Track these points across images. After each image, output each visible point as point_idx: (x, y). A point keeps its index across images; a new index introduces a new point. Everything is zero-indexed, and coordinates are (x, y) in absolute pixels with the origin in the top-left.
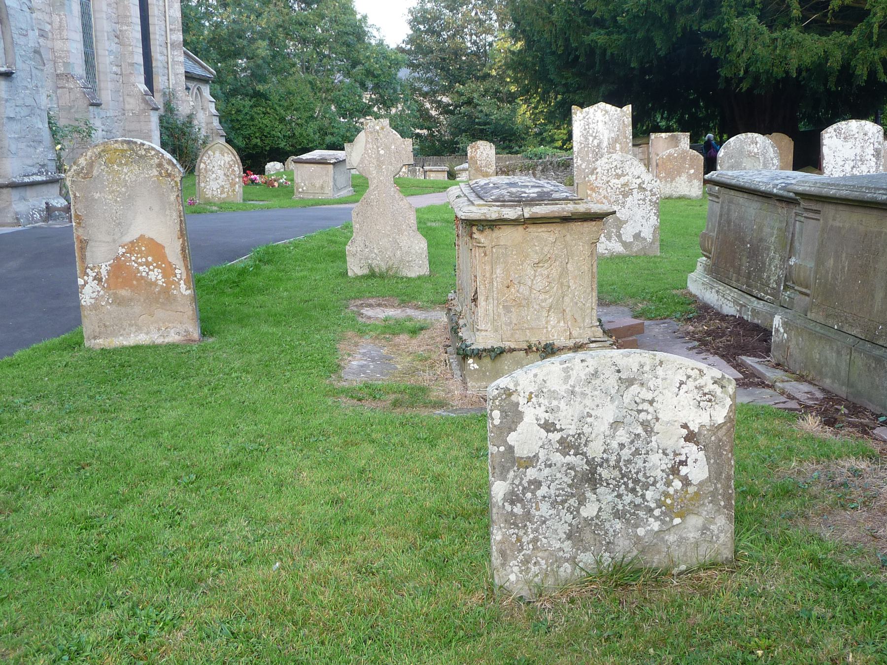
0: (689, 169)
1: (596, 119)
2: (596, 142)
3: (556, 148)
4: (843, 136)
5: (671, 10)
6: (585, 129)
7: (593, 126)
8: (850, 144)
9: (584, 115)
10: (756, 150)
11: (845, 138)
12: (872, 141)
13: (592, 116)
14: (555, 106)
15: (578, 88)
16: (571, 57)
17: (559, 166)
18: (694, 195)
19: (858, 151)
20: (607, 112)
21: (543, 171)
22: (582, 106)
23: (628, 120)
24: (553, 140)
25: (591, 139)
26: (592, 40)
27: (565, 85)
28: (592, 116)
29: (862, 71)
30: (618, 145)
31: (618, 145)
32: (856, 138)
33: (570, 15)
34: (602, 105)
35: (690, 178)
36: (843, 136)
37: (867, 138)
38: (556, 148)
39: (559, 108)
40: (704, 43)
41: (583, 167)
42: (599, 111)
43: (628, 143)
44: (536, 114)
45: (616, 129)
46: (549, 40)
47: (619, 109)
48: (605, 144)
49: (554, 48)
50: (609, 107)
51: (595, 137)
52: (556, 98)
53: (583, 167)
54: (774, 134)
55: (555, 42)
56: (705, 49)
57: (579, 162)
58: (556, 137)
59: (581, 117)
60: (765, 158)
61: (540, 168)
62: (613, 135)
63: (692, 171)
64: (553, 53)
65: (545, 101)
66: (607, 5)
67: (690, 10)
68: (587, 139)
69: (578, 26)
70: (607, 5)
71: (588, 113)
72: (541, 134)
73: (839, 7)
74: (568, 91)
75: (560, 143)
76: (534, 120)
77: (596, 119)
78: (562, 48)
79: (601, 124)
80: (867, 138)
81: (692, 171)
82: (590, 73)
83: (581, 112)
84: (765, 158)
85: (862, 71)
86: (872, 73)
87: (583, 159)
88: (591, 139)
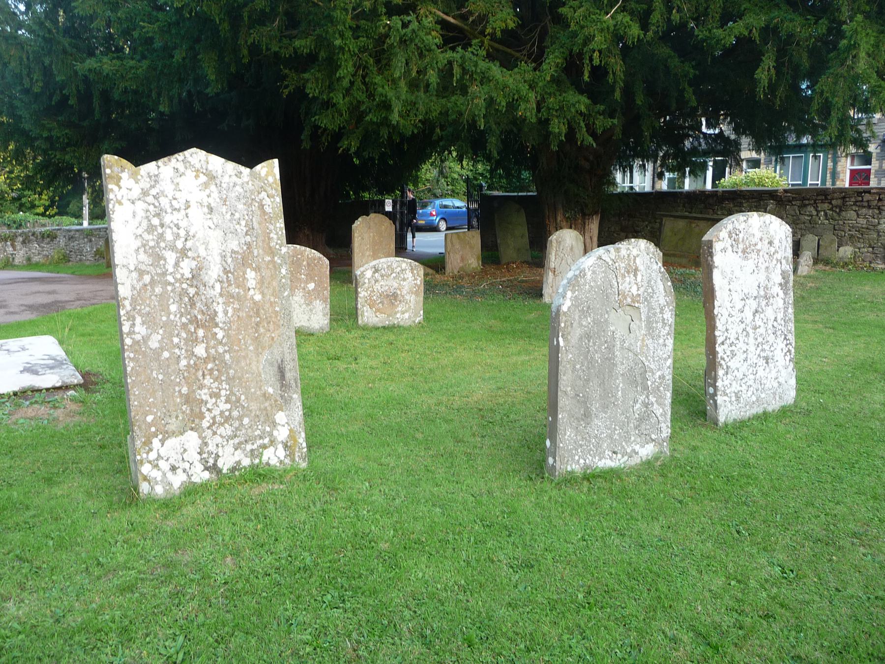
0: (307, 283)
1: (182, 197)
2: (186, 267)
3: (38, 214)
4: (741, 246)
5: (234, 15)
6: (151, 229)
7: (176, 217)
8: (750, 264)
9: (145, 184)
10: (634, 291)
11: (744, 252)
12: (778, 256)
13: (169, 189)
14: (35, 168)
15: (68, 145)
16: (56, 99)
17: (43, 237)
18: (317, 326)
19: (762, 277)
20: (211, 177)
21: (24, 242)
22: (139, 153)
23: (274, 202)
24: (33, 206)
25: (171, 257)
26: (90, 70)
27: (49, 139)
28: (169, 189)
29: (558, 127)
30: (251, 274)
31: (251, 274)
32: (759, 251)
33: (50, 31)
34: (196, 156)
35: (309, 297)
36: (741, 246)
37: (772, 250)
38: (38, 214)
39: (40, 171)
40: (285, 77)
41: (154, 343)
42: (190, 174)
43: (277, 268)
44: (12, 179)
45: (242, 228)
46: (17, 71)
47: (246, 171)
48: (214, 272)
49: (27, 83)
50: (216, 162)
51: (183, 253)
52: (34, 159)
53: (154, 343)
54: (372, 215)
55: (28, 75)
56: (286, 87)
57: (140, 329)
58: (37, 203)
59: (136, 192)
60: (650, 308)
61: (21, 239)
62: (234, 245)
63: (311, 286)
64: (27, 91)
65: (20, 163)
66: (115, 7)
67: (262, 18)
68: (158, 258)
69: (65, 52)
70: (115, 7)
71: (155, 179)
72: (19, 198)
73: (502, 31)
74: (52, 148)
75: (41, 210)
76: (9, 185)
77: (182, 197)
78: (40, 84)
79: (197, 215)
80: (772, 250)
81: (311, 286)
82: (86, 123)
83: (134, 176)
84: (650, 308)
85: (558, 127)
86: (571, 133)
87: (150, 322)
88: (171, 257)
